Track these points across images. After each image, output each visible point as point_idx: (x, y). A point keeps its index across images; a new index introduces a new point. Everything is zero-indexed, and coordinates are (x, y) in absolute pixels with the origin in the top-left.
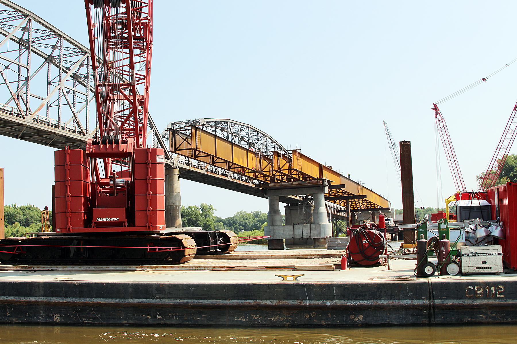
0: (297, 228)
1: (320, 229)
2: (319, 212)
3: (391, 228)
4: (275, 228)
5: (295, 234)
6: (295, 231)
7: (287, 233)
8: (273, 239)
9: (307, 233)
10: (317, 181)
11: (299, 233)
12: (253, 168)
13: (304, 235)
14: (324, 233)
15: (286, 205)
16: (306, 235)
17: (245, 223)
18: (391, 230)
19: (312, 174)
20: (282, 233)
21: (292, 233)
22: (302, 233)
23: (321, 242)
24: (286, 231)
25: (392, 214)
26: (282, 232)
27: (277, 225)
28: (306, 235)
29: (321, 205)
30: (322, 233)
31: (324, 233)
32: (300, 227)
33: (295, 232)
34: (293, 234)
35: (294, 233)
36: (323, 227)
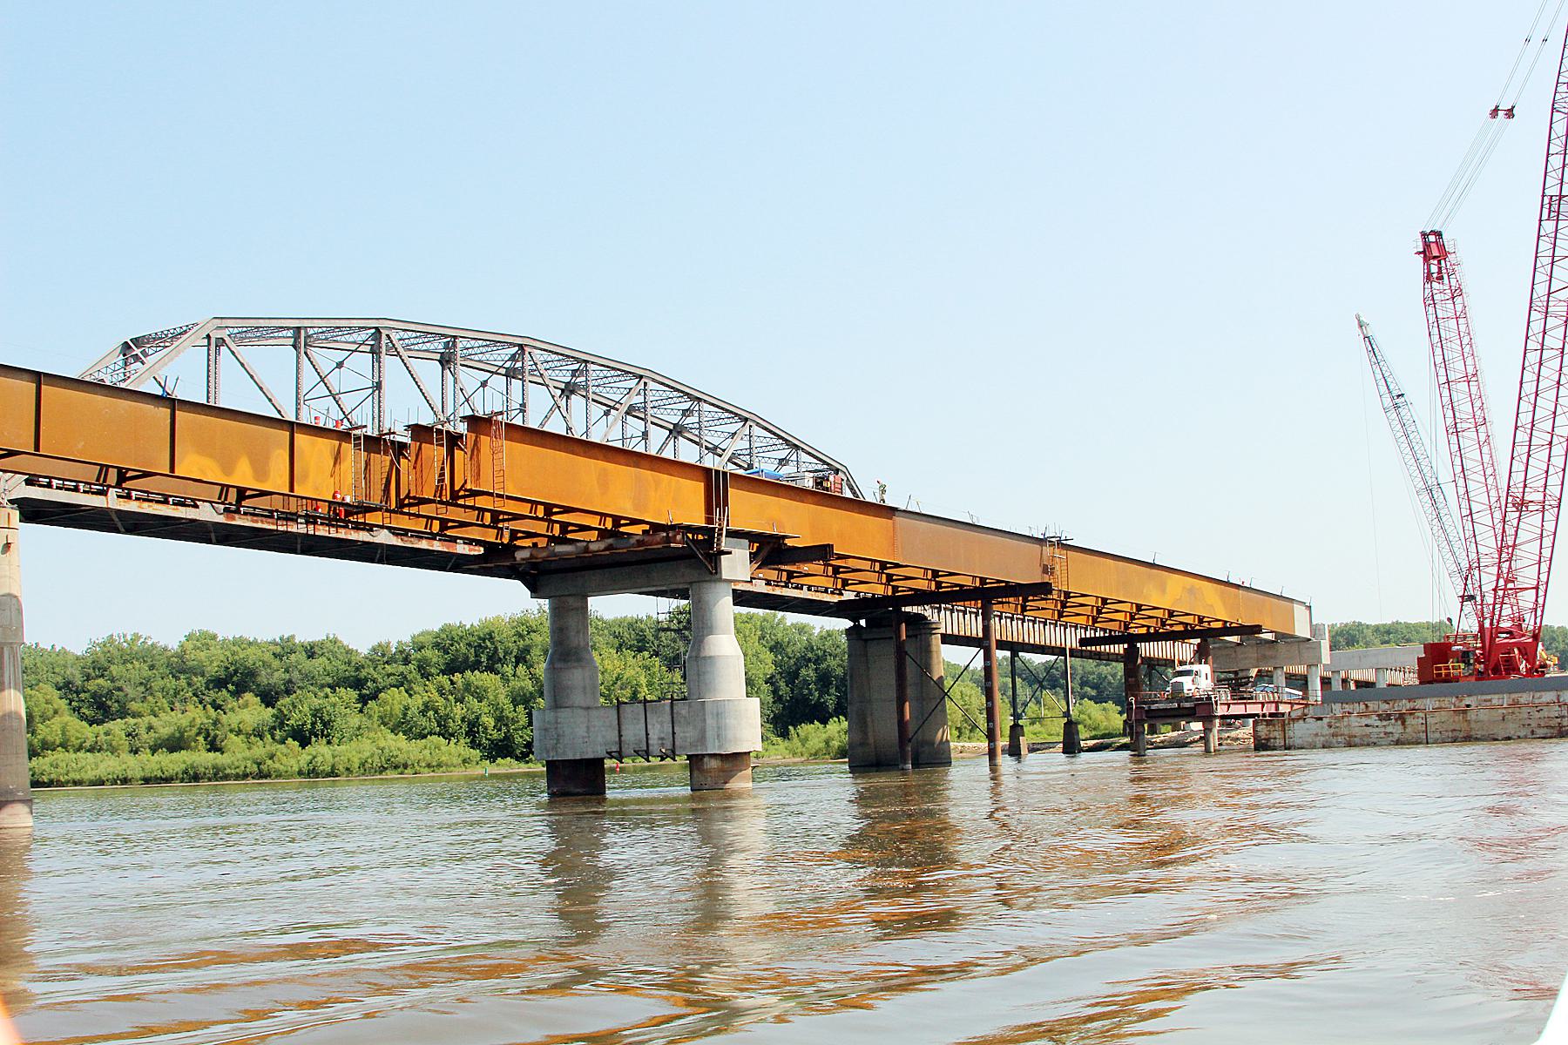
0: (630, 716)
1: (705, 720)
2: (702, 655)
3: (1187, 705)
4: (564, 714)
5: (622, 738)
6: (623, 727)
7: (597, 736)
8: (555, 759)
9: (662, 735)
10: (665, 534)
11: (635, 735)
12: (336, 492)
13: (653, 745)
14: (718, 736)
15: (852, 624)
16: (660, 742)
17: (1100, 674)
18: (1185, 712)
19: (637, 508)
20: (583, 737)
21: (614, 736)
22: (647, 734)
23: (708, 771)
24: (597, 728)
25: (1313, 646)
26: (581, 731)
27: (570, 703)
28: (660, 742)
29: (711, 627)
30: (710, 734)
31: (718, 736)
32: (638, 714)
33: (622, 733)
34: (617, 739)
35: (620, 736)
36: (715, 712)
